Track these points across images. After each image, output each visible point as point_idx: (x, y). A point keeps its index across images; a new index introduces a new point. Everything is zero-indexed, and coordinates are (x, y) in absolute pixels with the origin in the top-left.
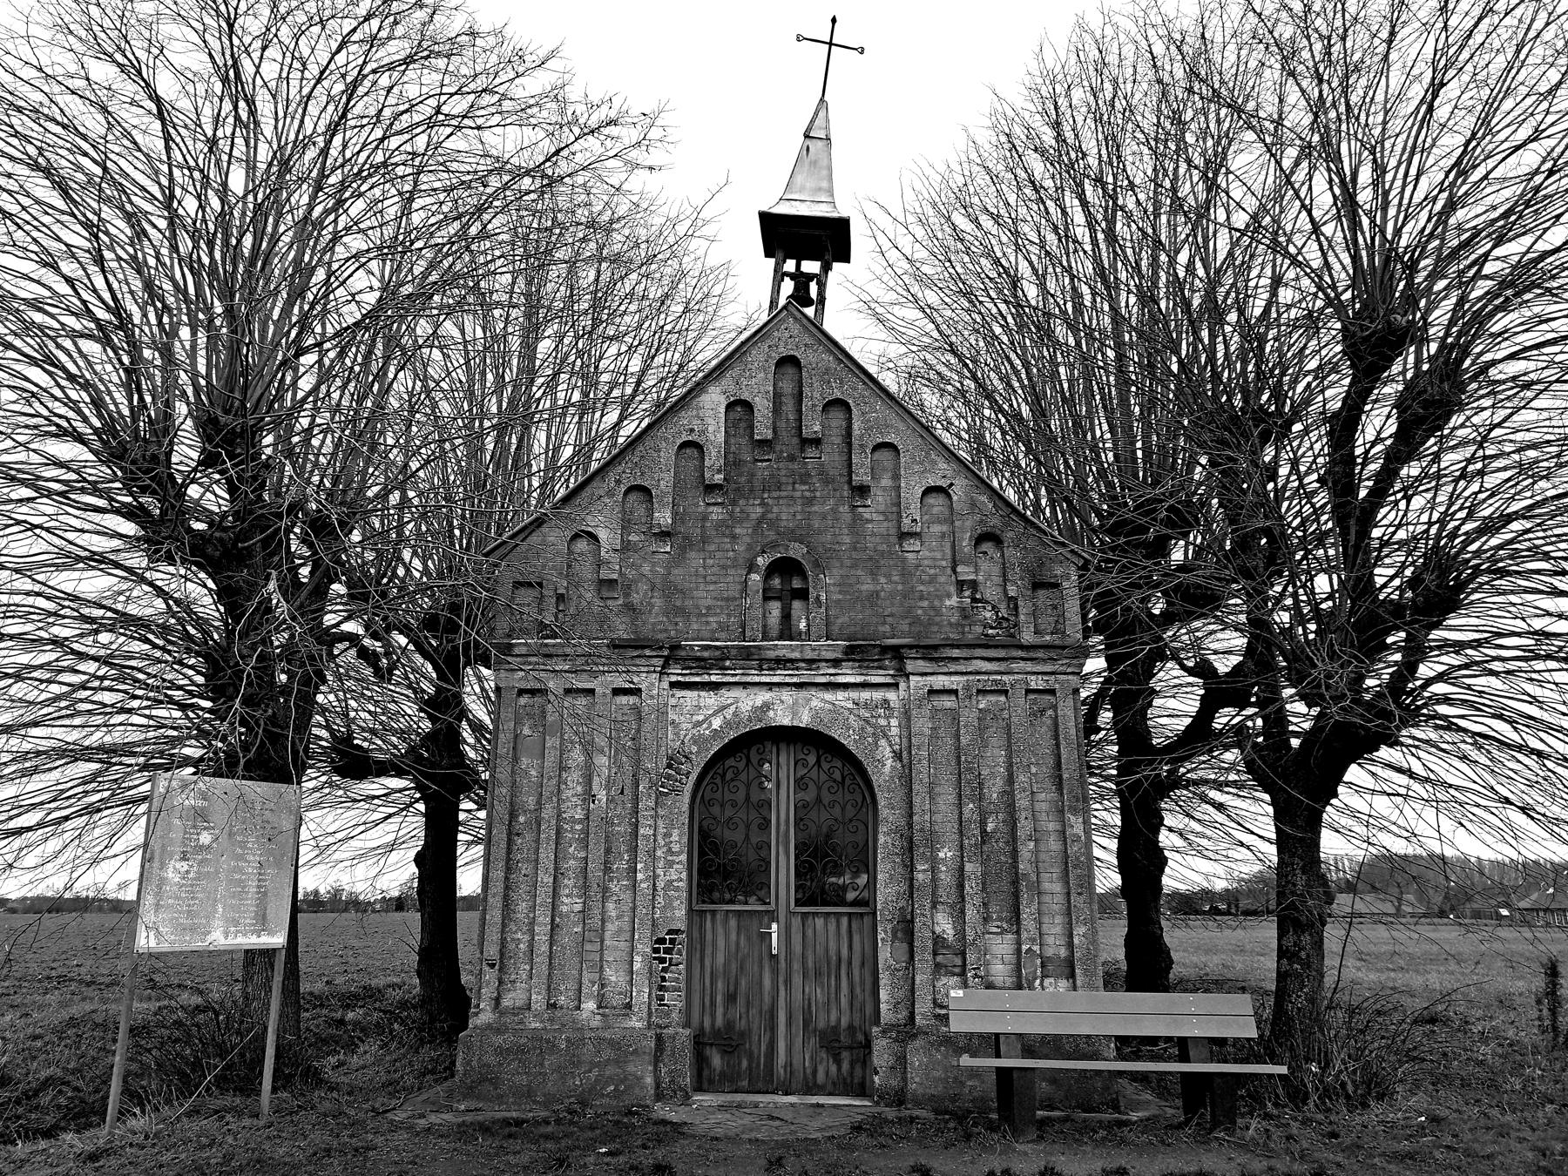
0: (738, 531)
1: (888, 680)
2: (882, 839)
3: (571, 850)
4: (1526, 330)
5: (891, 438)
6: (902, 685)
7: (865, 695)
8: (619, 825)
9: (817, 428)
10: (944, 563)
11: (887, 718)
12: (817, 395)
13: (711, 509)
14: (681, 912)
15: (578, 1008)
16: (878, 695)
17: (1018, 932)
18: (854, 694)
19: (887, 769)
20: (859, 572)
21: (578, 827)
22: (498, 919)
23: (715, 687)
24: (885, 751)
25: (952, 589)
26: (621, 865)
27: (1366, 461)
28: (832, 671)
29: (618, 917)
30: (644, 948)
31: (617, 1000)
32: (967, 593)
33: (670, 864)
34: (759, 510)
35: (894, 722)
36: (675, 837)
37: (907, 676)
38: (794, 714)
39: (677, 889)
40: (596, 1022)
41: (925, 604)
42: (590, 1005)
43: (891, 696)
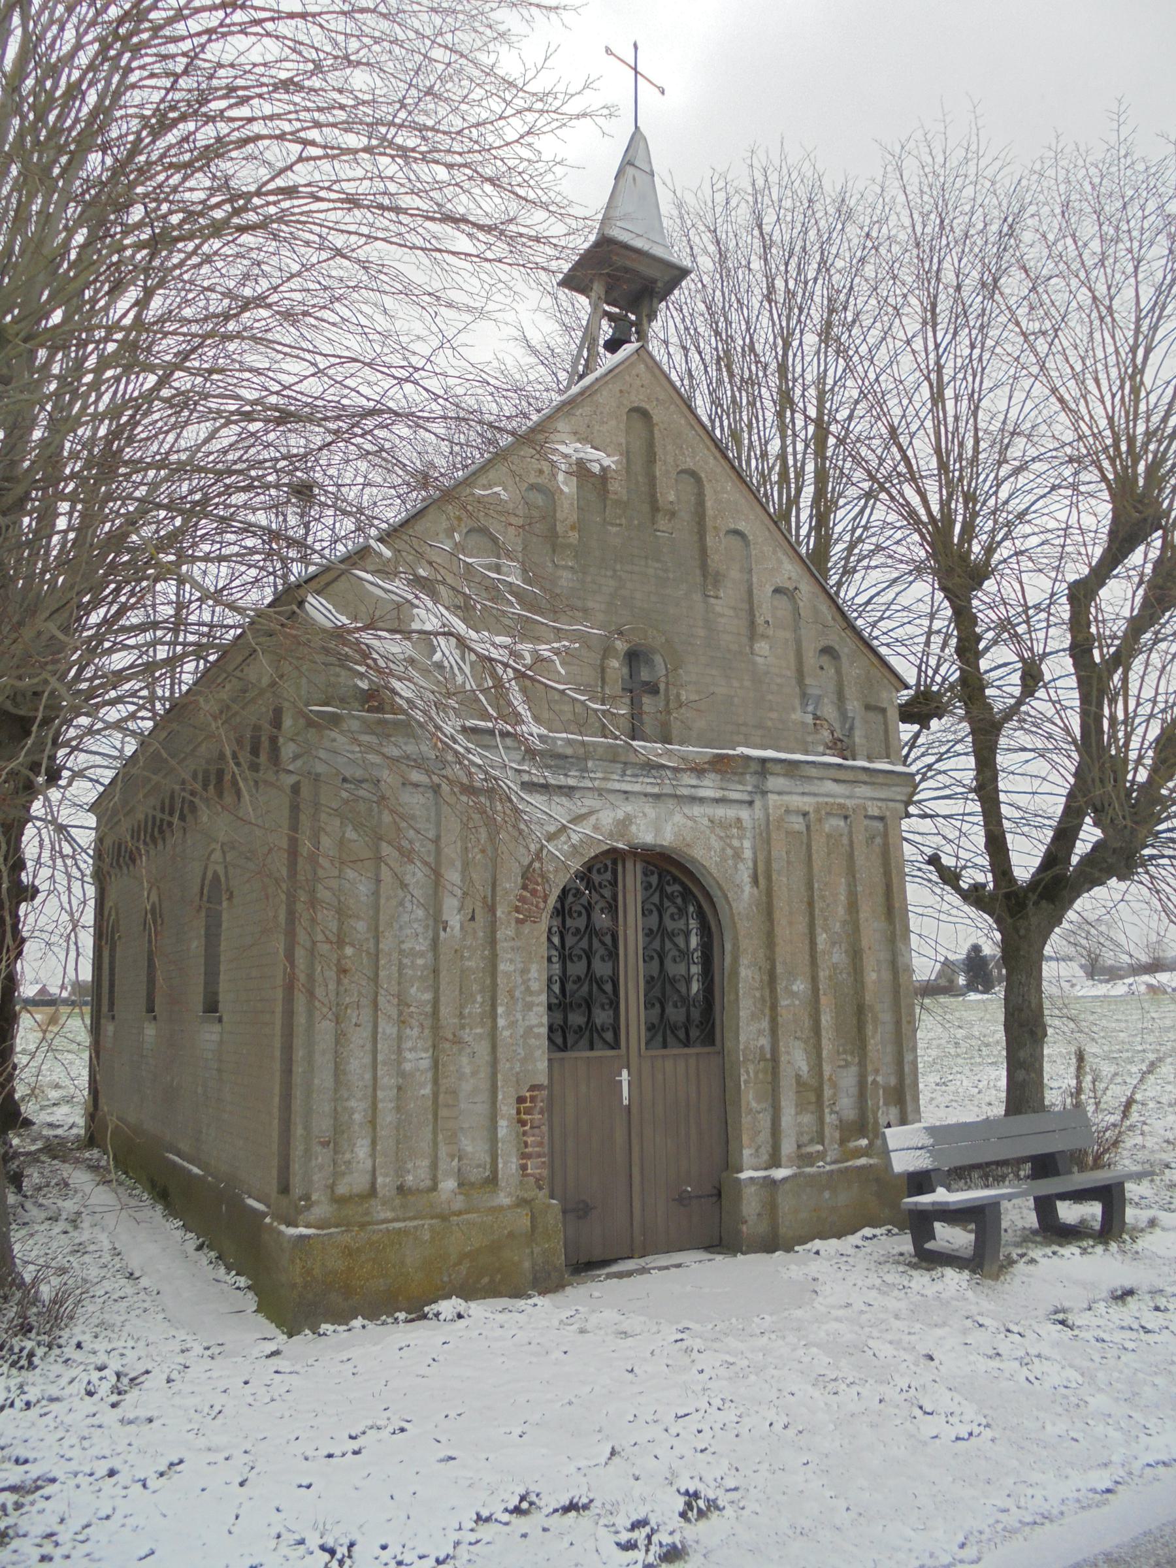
0: (590, 604)
1: (746, 797)
2: (744, 972)
3: (413, 990)
4: (1148, 351)
5: (742, 526)
6: (758, 804)
7: (720, 812)
8: (469, 959)
9: (672, 498)
10: (789, 673)
11: (741, 838)
12: (670, 460)
13: (560, 572)
14: (542, 1065)
15: (434, 1188)
16: (730, 812)
17: (862, 1064)
18: (710, 810)
19: (746, 895)
20: (714, 672)
21: (420, 962)
22: (329, 1082)
23: (568, 791)
24: (745, 876)
25: (797, 702)
26: (476, 1008)
27: (837, 541)
28: (694, 782)
29: (474, 1074)
30: (507, 1109)
31: (476, 1175)
32: (810, 708)
33: (529, 1006)
34: (612, 583)
35: (747, 844)
36: (534, 974)
37: (764, 793)
38: (658, 831)
39: (537, 1036)
40: (459, 1203)
41: (774, 715)
42: (449, 1185)
43: (745, 814)
